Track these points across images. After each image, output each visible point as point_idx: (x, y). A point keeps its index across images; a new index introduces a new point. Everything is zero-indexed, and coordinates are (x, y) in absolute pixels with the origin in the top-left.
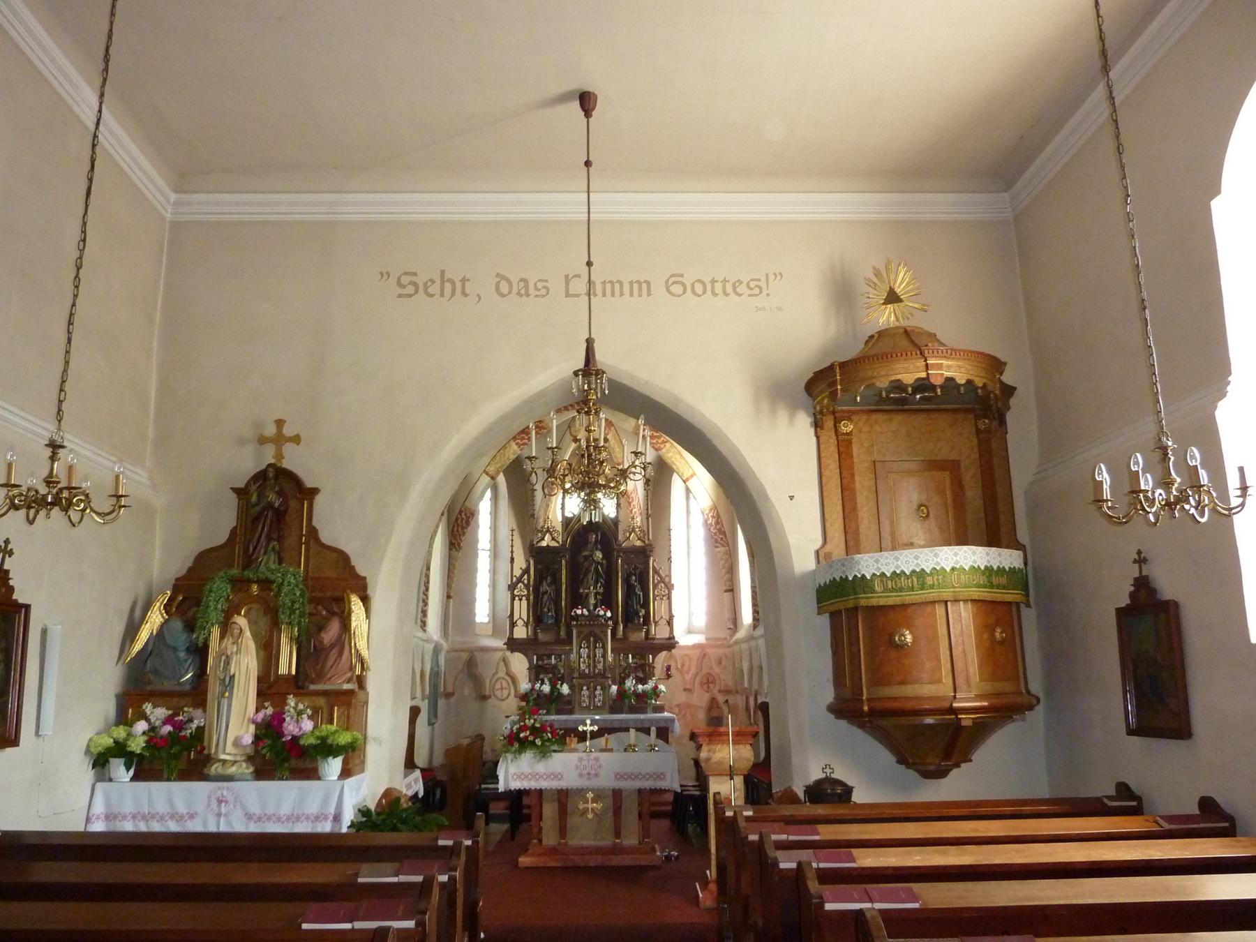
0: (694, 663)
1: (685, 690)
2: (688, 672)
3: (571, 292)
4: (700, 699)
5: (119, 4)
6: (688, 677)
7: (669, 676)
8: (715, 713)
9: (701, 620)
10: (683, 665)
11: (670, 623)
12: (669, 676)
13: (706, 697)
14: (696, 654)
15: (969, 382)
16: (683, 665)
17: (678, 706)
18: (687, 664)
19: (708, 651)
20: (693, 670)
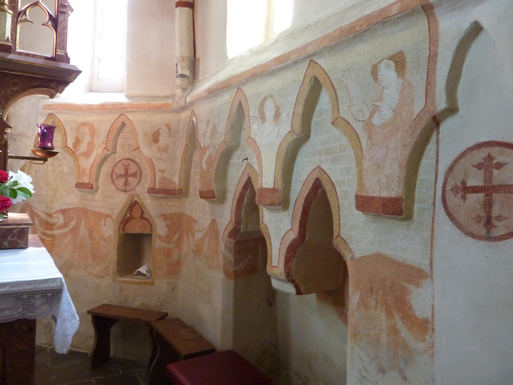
0: (100, 142)
1: (79, 185)
2: (87, 154)
3: (394, 191)
4: (110, 201)
5: (512, 241)
6: (87, 163)
7: (47, 153)
8: (135, 228)
9: (139, 57)
10: (77, 142)
11: (57, 22)
12: (47, 153)
13: (121, 200)
14: (104, 123)
15: (6, 214)
16: (77, 142)
17: (63, 212)
18: (87, 140)
19: (131, 116)
20: (98, 152)
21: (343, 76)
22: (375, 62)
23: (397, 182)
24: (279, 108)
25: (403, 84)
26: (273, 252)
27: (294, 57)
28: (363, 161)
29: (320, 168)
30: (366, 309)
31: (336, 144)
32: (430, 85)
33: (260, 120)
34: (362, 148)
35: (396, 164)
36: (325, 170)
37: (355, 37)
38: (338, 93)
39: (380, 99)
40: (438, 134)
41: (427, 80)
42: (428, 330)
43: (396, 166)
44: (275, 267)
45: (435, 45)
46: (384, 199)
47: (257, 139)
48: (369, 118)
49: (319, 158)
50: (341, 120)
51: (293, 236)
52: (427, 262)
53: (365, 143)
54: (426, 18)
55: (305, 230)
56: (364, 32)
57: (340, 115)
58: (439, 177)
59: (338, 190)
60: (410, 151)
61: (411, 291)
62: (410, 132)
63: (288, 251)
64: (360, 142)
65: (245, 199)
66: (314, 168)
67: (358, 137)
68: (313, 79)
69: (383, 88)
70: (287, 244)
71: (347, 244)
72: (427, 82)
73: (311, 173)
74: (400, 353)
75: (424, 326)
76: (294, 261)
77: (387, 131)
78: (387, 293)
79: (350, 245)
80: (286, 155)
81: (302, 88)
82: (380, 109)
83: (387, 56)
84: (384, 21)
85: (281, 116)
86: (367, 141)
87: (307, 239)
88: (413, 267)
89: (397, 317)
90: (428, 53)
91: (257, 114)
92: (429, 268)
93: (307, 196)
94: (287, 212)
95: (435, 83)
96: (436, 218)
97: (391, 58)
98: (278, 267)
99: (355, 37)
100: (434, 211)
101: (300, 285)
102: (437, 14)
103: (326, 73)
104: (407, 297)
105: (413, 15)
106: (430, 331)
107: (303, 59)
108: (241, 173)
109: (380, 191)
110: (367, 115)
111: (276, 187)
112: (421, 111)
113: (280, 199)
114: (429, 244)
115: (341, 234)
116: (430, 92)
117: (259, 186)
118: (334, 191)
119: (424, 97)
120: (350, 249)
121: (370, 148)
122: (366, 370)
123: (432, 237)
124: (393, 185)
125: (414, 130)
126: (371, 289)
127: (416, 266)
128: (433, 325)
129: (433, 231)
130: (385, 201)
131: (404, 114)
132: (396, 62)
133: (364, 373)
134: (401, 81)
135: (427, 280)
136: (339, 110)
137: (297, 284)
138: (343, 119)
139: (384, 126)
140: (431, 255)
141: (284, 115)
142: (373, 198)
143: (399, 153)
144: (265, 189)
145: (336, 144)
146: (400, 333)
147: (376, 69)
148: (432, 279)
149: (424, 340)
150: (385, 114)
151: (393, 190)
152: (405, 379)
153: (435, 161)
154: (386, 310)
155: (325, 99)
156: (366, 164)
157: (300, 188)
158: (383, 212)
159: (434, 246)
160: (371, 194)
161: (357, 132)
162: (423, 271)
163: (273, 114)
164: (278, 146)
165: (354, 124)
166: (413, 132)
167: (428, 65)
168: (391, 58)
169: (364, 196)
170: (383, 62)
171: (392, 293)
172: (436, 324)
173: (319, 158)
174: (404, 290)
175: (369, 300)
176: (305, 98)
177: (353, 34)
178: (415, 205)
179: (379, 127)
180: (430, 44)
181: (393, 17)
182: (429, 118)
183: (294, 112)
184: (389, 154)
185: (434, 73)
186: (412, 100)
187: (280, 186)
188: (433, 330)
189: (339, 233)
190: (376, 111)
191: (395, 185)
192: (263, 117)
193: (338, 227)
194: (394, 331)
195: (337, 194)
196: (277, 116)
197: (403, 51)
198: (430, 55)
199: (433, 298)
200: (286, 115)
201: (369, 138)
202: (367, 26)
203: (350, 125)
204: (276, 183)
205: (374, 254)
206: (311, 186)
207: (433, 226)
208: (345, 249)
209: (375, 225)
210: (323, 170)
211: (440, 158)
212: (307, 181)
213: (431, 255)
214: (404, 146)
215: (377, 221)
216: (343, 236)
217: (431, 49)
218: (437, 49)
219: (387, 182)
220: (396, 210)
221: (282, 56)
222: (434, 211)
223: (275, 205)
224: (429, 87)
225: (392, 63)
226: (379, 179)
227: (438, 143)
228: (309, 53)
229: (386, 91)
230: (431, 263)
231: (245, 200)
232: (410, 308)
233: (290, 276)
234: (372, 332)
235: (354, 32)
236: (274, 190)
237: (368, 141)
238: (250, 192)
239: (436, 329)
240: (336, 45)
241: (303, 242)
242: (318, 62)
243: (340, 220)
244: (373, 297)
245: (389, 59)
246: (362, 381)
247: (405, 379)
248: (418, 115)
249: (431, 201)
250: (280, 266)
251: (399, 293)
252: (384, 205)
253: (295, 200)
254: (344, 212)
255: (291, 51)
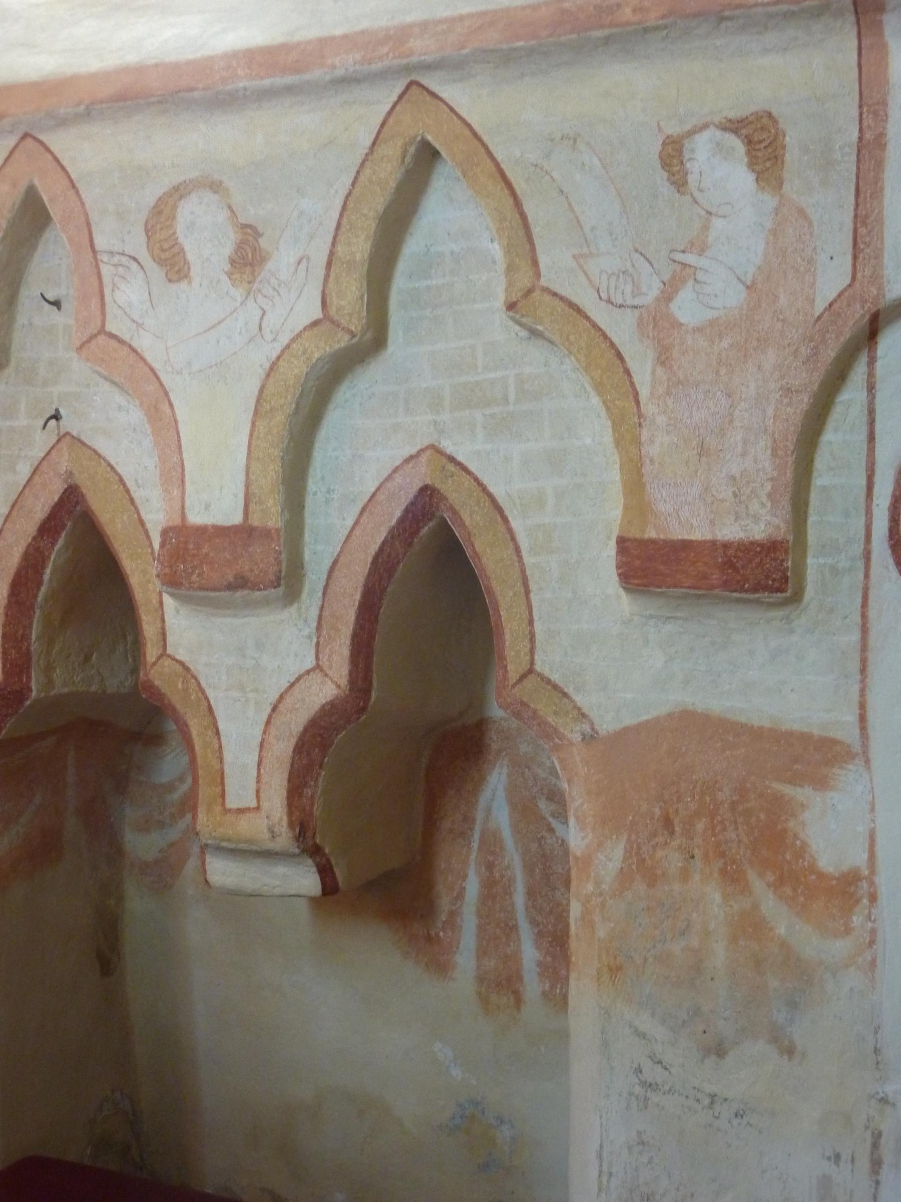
3: (759, 523)
21: (548, 156)
22: (673, 129)
23: (769, 495)
24: (257, 234)
25: (777, 211)
26: (228, 756)
27: (346, 62)
28: (645, 434)
29: (439, 452)
30: (652, 884)
31: (499, 374)
32: (864, 224)
33: (157, 273)
34: (636, 394)
35: (762, 443)
36: (460, 458)
37: (607, 41)
38: (529, 208)
39: (700, 246)
40: (872, 361)
41: (856, 209)
42: (858, 901)
43: (761, 449)
44: (241, 811)
45: (876, 114)
46: (726, 546)
47: (145, 343)
48: (657, 299)
49: (430, 417)
50: (547, 298)
51: (324, 691)
52: (851, 717)
53: (648, 377)
54: (854, 33)
55: (368, 669)
56: (646, 30)
57: (543, 282)
58: (877, 479)
59: (515, 524)
60: (805, 407)
61: (802, 805)
62: (804, 351)
63: (299, 749)
64: (627, 372)
65: (48, 571)
66: (414, 451)
67: (619, 356)
68: (412, 150)
69: (710, 213)
70: (296, 720)
71: (565, 695)
72: (856, 216)
73: (396, 470)
74: (774, 983)
75: (848, 891)
76: (321, 780)
77: (725, 344)
78: (722, 822)
79: (578, 699)
80: (297, 404)
81: (367, 172)
82: (700, 276)
83: (717, 119)
84: (726, 13)
85: (270, 265)
86: (653, 373)
87: (374, 695)
88: (805, 738)
89: (758, 884)
90: (856, 134)
91: (137, 243)
92: (857, 731)
93: (381, 550)
94: (293, 609)
95: (880, 221)
96: (872, 594)
97: (734, 126)
98: (258, 808)
99: (607, 41)
100: (867, 576)
101: (333, 861)
102: (888, 32)
103: (475, 134)
104: (791, 824)
105: (818, 16)
106: (865, 901)
107: (383, 75)
108: (24, 470)
109: (712, 523)
110: (652, 289)
111: (255, 521)
112: (840, 295)
113: (279, 563)
114: (854, 666)
115: (538, 667)
116: (868, 245)
117: (156, 516)
118: (502, 528)
119: (849, 258)
120: (579, 709)
121: (668, 393)
122: (660, 1062)
123: (864, 647)
124: (754, 506)
125: (815, 347)
126: (668, 823)
127: (816, 732)
128: (872, 883)
129: (864, 630)
130: (731, 552)
131: (783, 300)
132: (749, 142)
133: (652, 1073)
134: (769, 201)
135: (851, 767)
136: (535, 263)
137: (328, 860)
138: (555, 294)
139: (714, 329)
140: (863, 692)
141: (282, 260)
142: (686, 545)
143: (770, 412)
144: (201, 531)
145: (499, 374)
146: (771, 929)
147: (680, 152)
148: (867, 761)
149: (848, 931)
150: (715, 293)
151: (756, 519)
152: (789, 1051)
153: (863, 436)
154: (723, 872)
155: (451, 216)
156: (657, 443)
157: (350, 522)
158: (726, 585)
159: (870, 669)
160: (678, 533)
161: (615, 340)
162: (834, 742)
163: (228, 250)
164: (261, 373)
165: (600, 315)
166: (815, 352)
167: (858, 168)
168: (734, 126)
169: (653, 541)
170: (706, 135)
171: (740, 820)
172: (881, 879)
173: (430, 417)
174: (779, 807)
175: (660, 853)
176: (381, 208)
177: (607, 32)
178: (809, 561)
179: (698, 330)
180: (861, 107)
181: (759, 9)
182: (863, 316)
183: (332, 254)
184: (737, 412)
185: (877, 193)
186: (811, 261)
187: (271, 515)
188: (873, 898)
189: (532, 663)
190: (684, 282)
191: (763, 505)
192: (174, 264)
193: (525, 646)
194: (750, 926)
195: (513, 539)
196: (248, 258)
197: (774, 113)
198: (860, 139)
199: (873, 810)
200: (293, 260)
201: (663, 358)
202: (663, 17)
203: (587, 318)
204: (253, 507)
205: (670, 716)
206: (398, 513)
207: (864, 616)
208: (556, 713)
209: (670, 627)
210: (452, 459)
211: (878, 426)
212: (381, 497)
213: (863, 692)
214: (787, 391)
215: (679, 614)
216: (546, 672)
217: (865, 123)
218: (885, 128)
219: (735, 495)
220: (767, 577)
221: (284, 48)
222: (867, 576)
223: (255, 587)
224: (862, 231)
225: (737, 145)
226: (707, 489)
227: (871, 388)
228: (415, 59)
229: (718, 223)
230: (863, 719)
231: (46, 577)
232: (801, 851)
233: (309, 834)
234: (676, 948)
235: (611, 25)
236: (244, 533)
237: (660, 371)
238: (66, 546)
239: (883, 892)
240: (531, 51)
241: (363, 709)
242: (443, 95)
243: (531, 622)
244: (675, 843)
245: (725, 129)
246: (646, 1099)
247: (789, 1051)
248: (831, 305)
249: (858, 549)
250: (265, 805)
251: (762, 816)
252: (729, 564)
253: (327, 563)
254: (548, 595)
255: (333, 39)
